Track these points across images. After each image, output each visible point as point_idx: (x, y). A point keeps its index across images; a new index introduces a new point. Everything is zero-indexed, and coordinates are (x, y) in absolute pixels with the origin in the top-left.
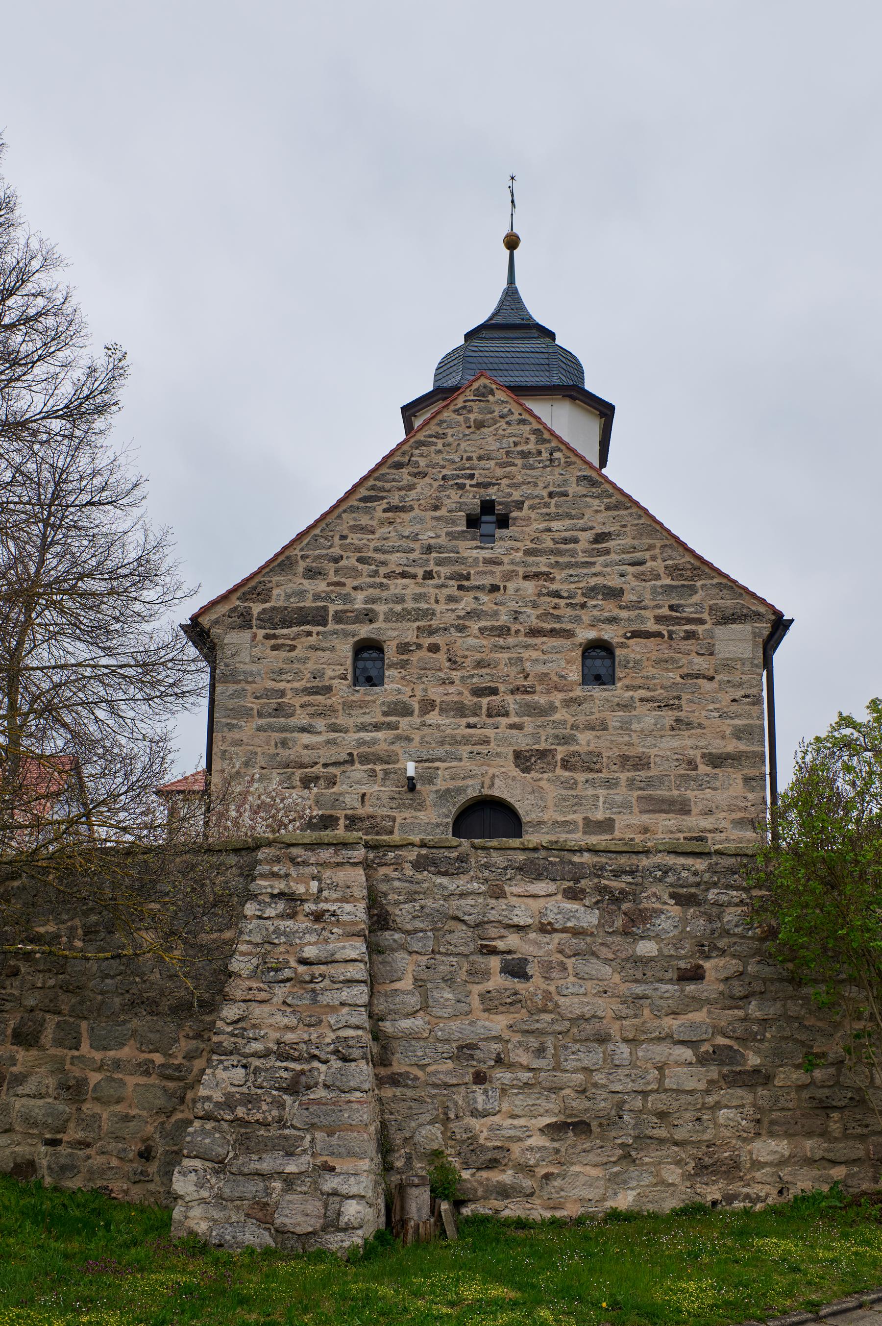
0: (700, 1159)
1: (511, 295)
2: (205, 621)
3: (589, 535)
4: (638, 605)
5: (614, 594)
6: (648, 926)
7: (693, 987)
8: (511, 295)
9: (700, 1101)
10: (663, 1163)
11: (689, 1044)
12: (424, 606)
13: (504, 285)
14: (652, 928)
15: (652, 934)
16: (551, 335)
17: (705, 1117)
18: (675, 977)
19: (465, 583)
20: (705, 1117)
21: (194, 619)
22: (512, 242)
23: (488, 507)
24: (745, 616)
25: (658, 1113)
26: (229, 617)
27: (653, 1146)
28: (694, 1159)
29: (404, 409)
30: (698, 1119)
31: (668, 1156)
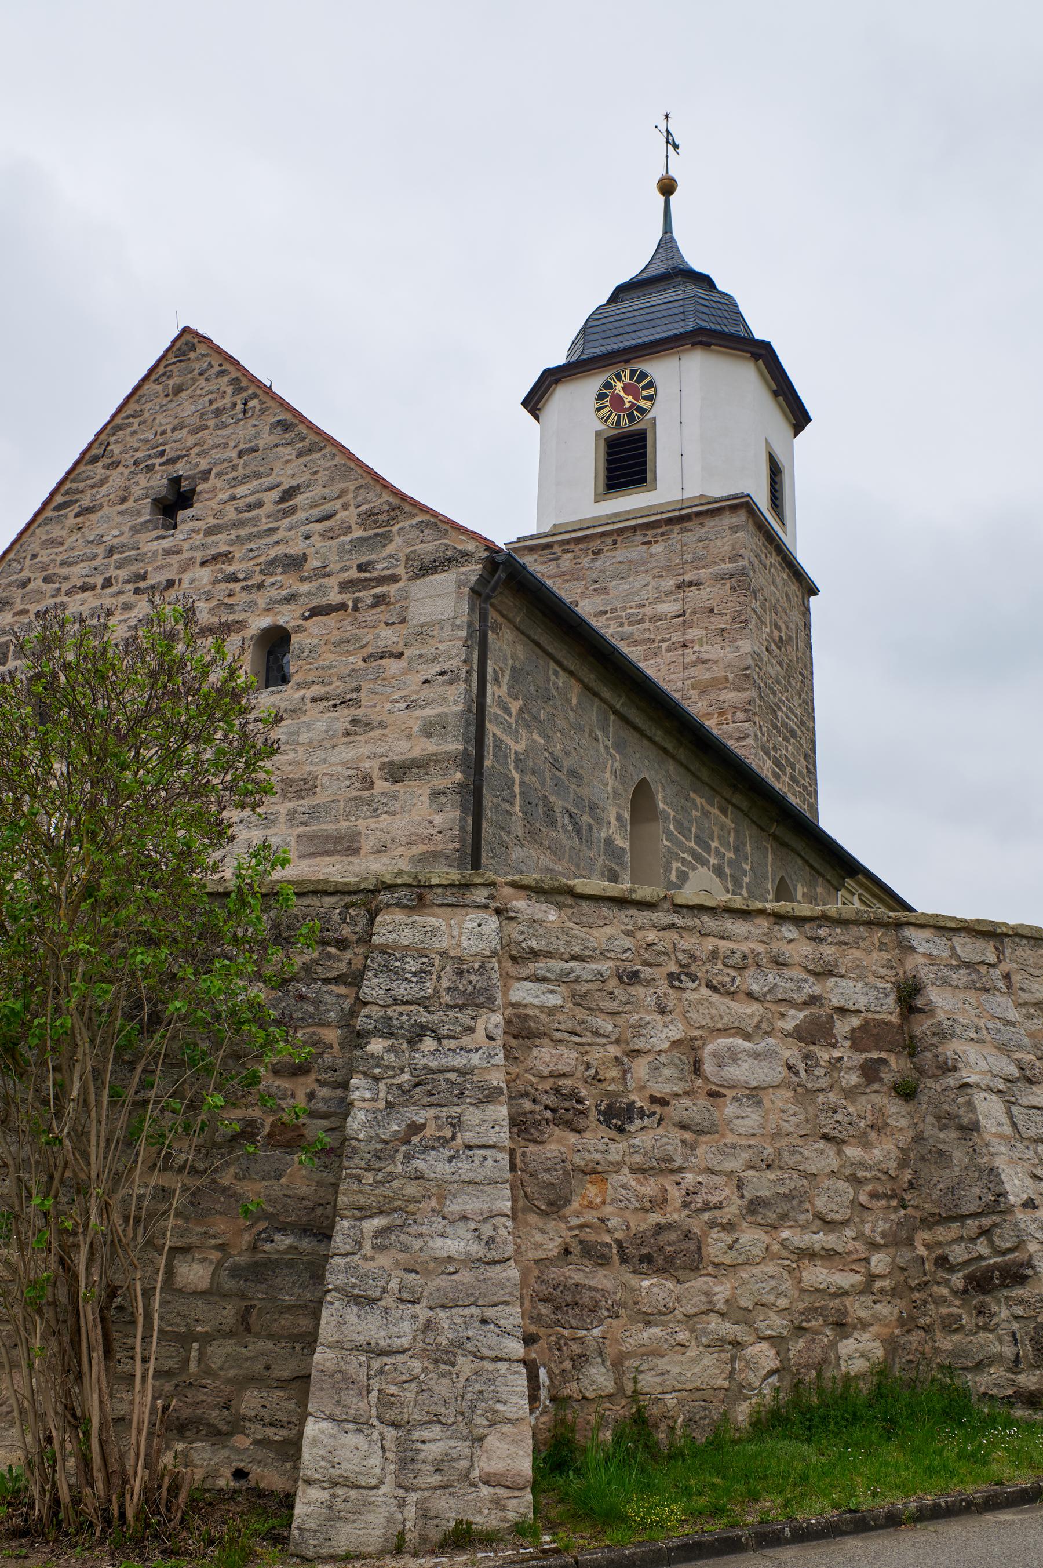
1: (667, 244)
3: (275, 494)
4: (323, 572)
5: (295, 563)
8: (667, 244)
16: (705, 281)
29: (525, 403)
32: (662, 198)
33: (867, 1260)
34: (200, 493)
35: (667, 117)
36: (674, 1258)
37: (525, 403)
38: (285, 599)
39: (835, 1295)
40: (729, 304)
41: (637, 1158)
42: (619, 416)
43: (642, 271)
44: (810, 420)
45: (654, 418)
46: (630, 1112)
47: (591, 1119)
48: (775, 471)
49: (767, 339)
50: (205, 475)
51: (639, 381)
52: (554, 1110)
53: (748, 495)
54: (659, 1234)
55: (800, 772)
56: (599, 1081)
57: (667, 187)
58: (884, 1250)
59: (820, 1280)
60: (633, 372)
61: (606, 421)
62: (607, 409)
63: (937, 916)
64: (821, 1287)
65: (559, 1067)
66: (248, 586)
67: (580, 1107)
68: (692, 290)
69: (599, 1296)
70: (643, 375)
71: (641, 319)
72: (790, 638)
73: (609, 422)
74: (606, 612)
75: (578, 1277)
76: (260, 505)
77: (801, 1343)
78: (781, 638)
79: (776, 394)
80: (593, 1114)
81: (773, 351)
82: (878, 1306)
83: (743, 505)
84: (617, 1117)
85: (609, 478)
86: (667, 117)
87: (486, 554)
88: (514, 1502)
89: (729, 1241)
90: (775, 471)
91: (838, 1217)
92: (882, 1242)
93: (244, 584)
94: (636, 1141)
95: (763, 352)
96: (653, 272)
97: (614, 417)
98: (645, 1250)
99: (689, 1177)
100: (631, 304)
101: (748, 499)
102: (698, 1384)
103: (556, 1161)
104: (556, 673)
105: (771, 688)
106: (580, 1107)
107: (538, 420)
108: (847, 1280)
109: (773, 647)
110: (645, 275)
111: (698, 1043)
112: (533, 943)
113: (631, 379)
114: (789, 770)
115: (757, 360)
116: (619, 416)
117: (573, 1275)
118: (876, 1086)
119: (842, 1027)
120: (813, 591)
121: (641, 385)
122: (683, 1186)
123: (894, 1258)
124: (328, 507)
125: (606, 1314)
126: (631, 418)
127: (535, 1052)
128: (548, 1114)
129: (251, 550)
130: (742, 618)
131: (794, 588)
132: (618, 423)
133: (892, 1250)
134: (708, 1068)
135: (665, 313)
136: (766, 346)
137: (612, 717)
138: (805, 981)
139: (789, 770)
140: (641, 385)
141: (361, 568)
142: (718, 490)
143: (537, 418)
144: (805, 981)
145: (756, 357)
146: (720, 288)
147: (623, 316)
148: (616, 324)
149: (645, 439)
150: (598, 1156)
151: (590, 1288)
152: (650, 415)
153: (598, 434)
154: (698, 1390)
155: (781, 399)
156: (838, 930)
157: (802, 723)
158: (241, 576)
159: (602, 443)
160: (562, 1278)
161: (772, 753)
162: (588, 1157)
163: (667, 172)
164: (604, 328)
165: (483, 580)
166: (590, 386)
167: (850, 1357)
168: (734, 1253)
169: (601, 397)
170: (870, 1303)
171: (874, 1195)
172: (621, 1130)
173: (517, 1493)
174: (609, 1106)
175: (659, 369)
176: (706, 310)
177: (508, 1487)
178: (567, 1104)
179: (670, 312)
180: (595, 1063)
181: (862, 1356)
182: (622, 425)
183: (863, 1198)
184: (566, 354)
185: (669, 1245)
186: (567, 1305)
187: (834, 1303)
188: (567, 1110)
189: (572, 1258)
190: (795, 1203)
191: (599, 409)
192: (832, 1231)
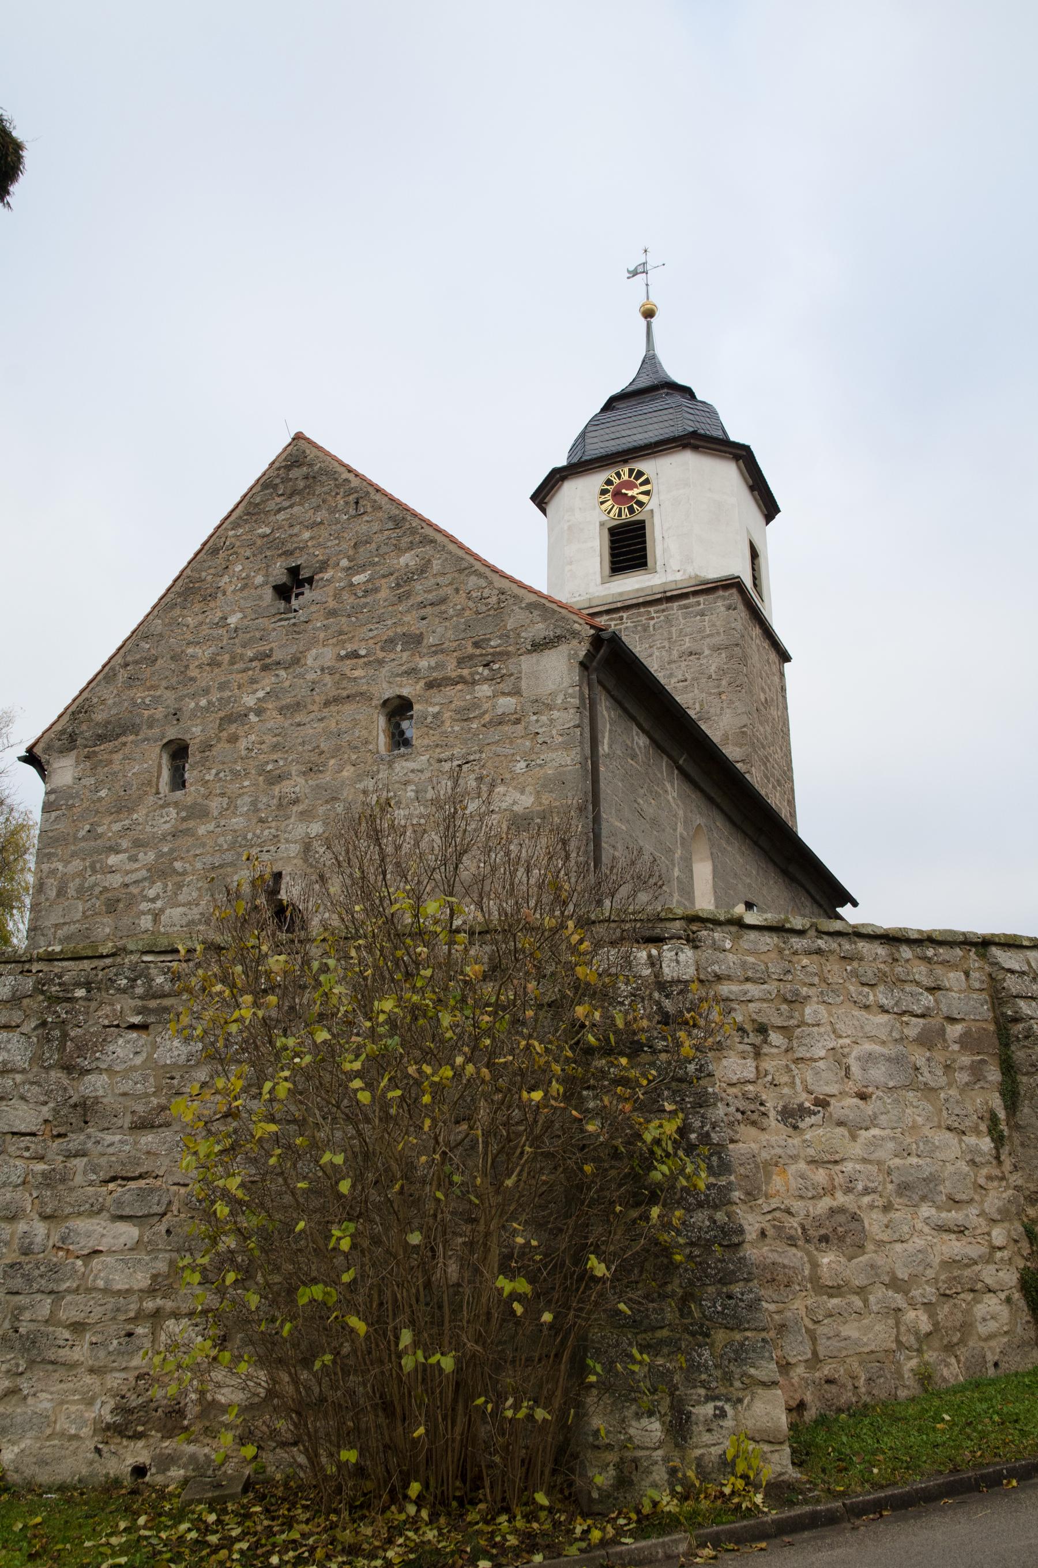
0: (123, 1397)
1: (650, 361)
2: (38, 750)
3: (392, 581)
4: (438, 650)
5: (414, 641)
6: (97, 1055)
7: (150, 1138)
8: (650, 361)
9: (134, 1307)
10: (67, 1402)
11: (135, 1220)
12: (227, 694)
13: (643, 353)
14: (103, 1057)
15: (103, 1066)
16: (687, 392)
17: (140, 1331)
18: (126, 1125)
19: (268, 661)
20: (140, 1331)
21: (30, 750)
22: (649, 314)
23: (294, 571)
24: (559, 637)
25: (72, 1324)
26: (60, 740)
27: (57, 1376)
28: (114, 1396)
29: (533, 498)
30: (130, 1335)
31: (75, 1392)
32: (643, 322)
33: (989, 1234)
34: (318, 581)
36: (845, 1237)
37: (533, 498)
38: (406, 672)
39: (968, 1266)
40: (709, 411)
41: (811, 1151)
42: (620, 509)
43: (631, 384)
45: (652, 511)
46: (802, 1112)
47: (772, 1118)
48: (754, 555)
49: (747, 443)
50: (324, 566)
51: (637, 478)
52: (743, 1113)
53: (739, 577)
54: (832, 1217)
56: (775, 1085)
58: (1000, 1224)
59: (955, 1252)
60: (631, 471)
62: (610, 502)
63: (1015, 935)
64: (957, 1258)
65: (745, 1074)
66: (370, 662)
67: (762, 1108)
68: (678, 399)
69: (791, 1273)
70: (640, 474)
71: (634, 424)
72: (772, 700)
73: (612, 515)
75: (773, 1257)
76: (376, 590)
77: (946, 1308)
78: (766, 699)
79: (752, 489)
80: (772, 1114)
81: (751, 453)
82: (1001, 1274)
83: (733, 584)
84: (792, 1116)
85: (612, 563)
87: (592, 632)
88: (776, 1455)
89: (885, 1221)
90: (754, 555)
91: (964, 1197)
92: (999, 1217)
93: (366, 659)
94: (807, 1137)
95: (744, 453)
96: (642, 384)
97: (615, 510)
98: (823, 1232)
99: (849, 1167)
100: (623, 411)
102: (873, 1347)
103: (748, 1156)
104: (637, 734)
105: (762, 744)
106: (762, 1108)
107: (545, 514)
108: (974, 1251)
109: (762, 708)
110: (631, 389)
111: (846, 1050)
112: (716, 968)
113: (630, 477)
116: (620, 509)
117: (770, 1255)
118: (982, 1084)
119: (955, 1031)
120: (785, 657)
122: (846, 1174)
123: (1009, 1231)
124: (442, 592)
125: (798, 1288)
126: (631, 510)
127: (725, 1062)
128: (739, 1116)
129: (371, 630)
130: (738, 683)
131: (773, 656)
132: (620, 515)
133: (1006, 1225)
134: (855, 1069)
135: (655, 420)
136: (746, 449)
137: (676, 772)
138: (921, 994)
141: (476, 645)
142: (714, 572)
143: (544, 511)
144: (921, 994)
145: (736, 458)
146: (699, 397)
147: (618, 422)
148: (613, 429)
149: (644, 528)
150: (779, 1151)
151: (784, 1266)
152: (648, 508)
153: (602, 524)
154: (872, 1352)
156: (941, 951)
157: (785, 773)
158: (363, 652)
159: (606, 533)
160: (761, 1258)
162: (773, 1152)
164: (602, 432)
165: (589, 655)
166: (596, 481)
167: (984, 1320)
168: (889, 1231)
169: (604, 492)
170: (994, 1272)
171: (990, 1178)
172: (795, 1127)
173: (777, 1447)
174: (785, 1107)
175: (647, 467)
176: (691, 417)
177: (770, 1442)
178: (752, 1107)
179: (660, 419)
180: (771, 1070)
181: (992, 1318)
182: (624, 517)
183: (982, 1181)
184: (566, 455)
185: (841, 1226)
186: (768, 1282)
187: (967, 1272)
188: (753, 1112)
189: (768, 1241)
190: (931, 1185)
191: (602, 503)
192: (960, 1209)
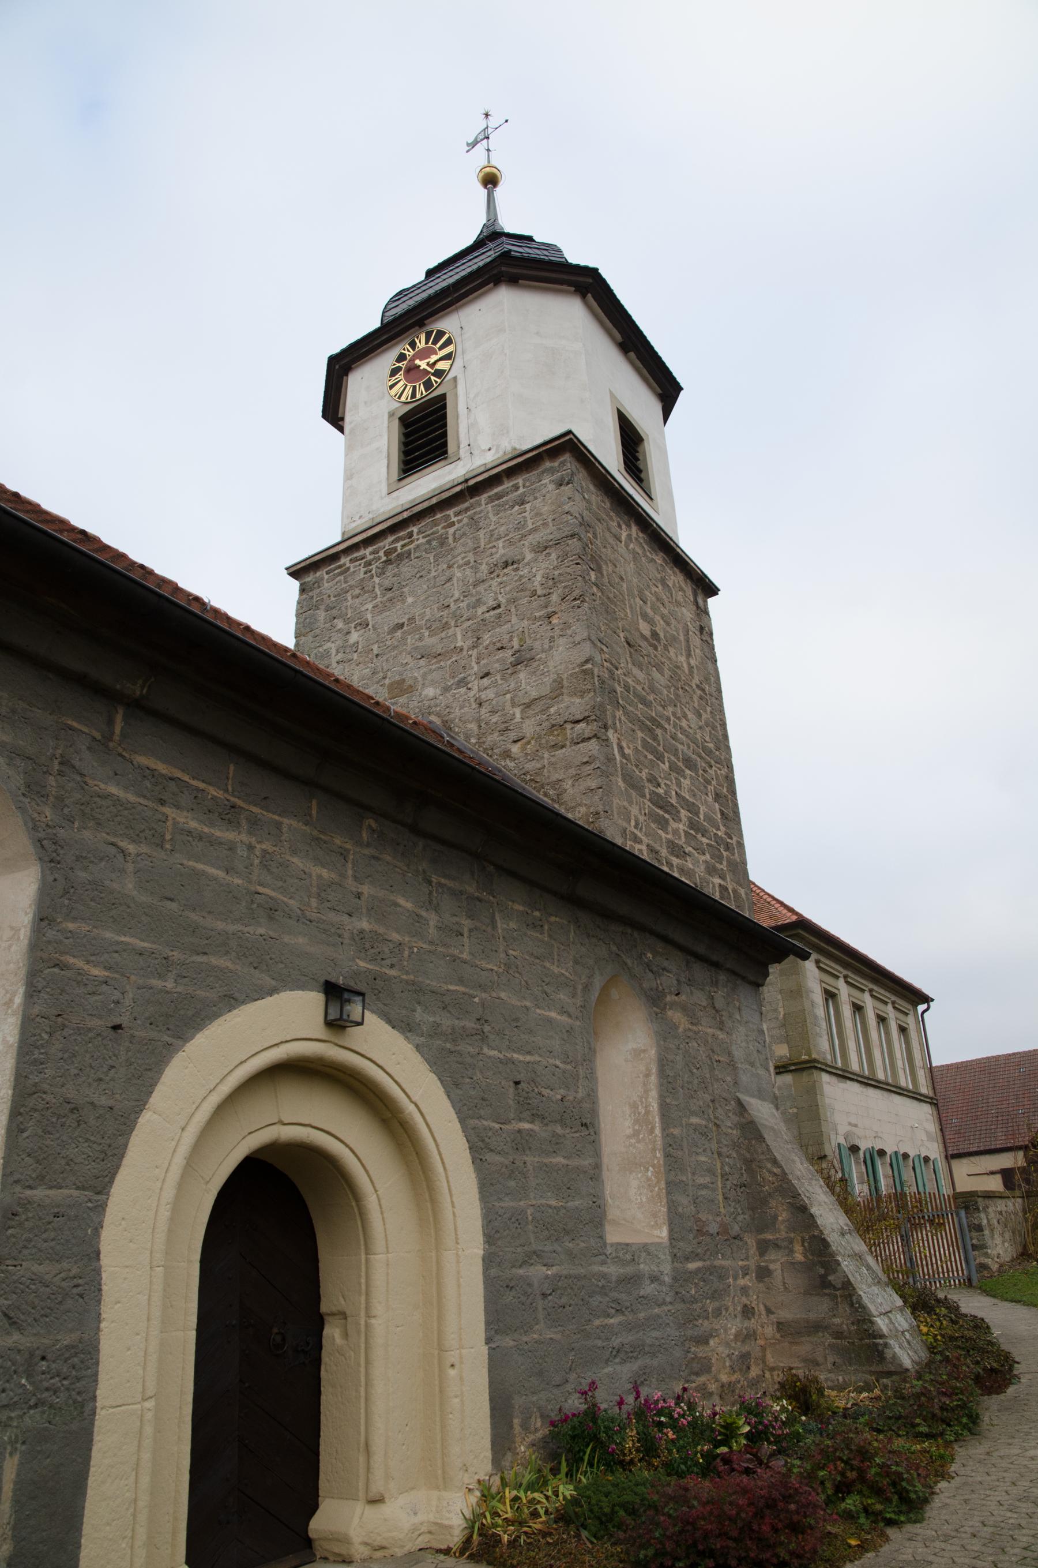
35: (487, 115)
42: (414, 387)
44: (682, 389)
55: (709, 818)
57: (490, 181)
60: (428, 335)
61: (399, 398)
62: (401, 383)
70: (441, 334)
73: (403, 399)
74: (402, 625)
86: (487, 115)
97: (409, 391)
101: (571, 436)
113: (427, 342)
114: (683, 813)
115: (584, 297)
116: (414, 387)
120: (712, 590)
121: (438, 345)
126: (428, 385)
132: (414, 395)
136: (593, 273)
139: (683, 813)
140: (438, 345)
153: (391, 415)
155: (632, 354)
159: (396, 423)
161: (649, 787)
163: (489, 162)
182: (418, 396)
